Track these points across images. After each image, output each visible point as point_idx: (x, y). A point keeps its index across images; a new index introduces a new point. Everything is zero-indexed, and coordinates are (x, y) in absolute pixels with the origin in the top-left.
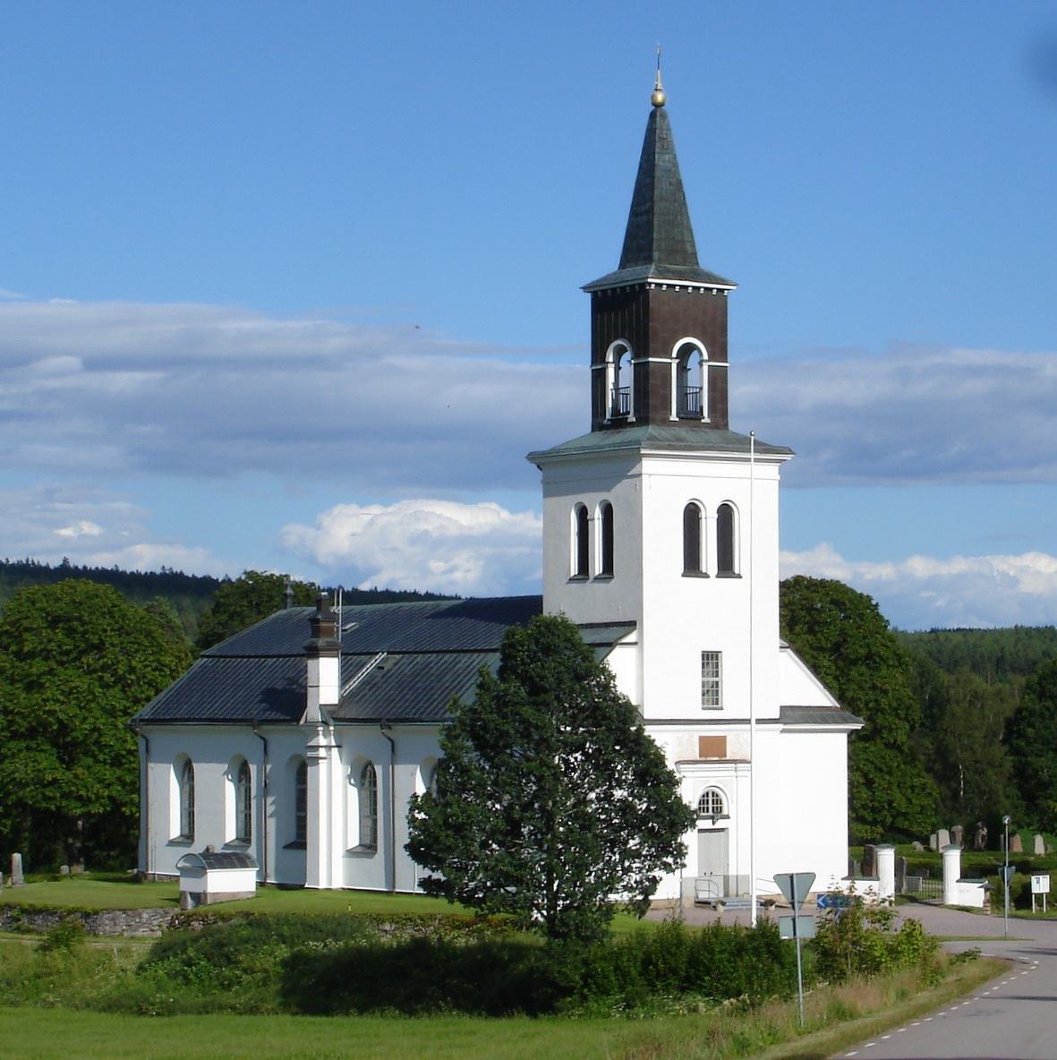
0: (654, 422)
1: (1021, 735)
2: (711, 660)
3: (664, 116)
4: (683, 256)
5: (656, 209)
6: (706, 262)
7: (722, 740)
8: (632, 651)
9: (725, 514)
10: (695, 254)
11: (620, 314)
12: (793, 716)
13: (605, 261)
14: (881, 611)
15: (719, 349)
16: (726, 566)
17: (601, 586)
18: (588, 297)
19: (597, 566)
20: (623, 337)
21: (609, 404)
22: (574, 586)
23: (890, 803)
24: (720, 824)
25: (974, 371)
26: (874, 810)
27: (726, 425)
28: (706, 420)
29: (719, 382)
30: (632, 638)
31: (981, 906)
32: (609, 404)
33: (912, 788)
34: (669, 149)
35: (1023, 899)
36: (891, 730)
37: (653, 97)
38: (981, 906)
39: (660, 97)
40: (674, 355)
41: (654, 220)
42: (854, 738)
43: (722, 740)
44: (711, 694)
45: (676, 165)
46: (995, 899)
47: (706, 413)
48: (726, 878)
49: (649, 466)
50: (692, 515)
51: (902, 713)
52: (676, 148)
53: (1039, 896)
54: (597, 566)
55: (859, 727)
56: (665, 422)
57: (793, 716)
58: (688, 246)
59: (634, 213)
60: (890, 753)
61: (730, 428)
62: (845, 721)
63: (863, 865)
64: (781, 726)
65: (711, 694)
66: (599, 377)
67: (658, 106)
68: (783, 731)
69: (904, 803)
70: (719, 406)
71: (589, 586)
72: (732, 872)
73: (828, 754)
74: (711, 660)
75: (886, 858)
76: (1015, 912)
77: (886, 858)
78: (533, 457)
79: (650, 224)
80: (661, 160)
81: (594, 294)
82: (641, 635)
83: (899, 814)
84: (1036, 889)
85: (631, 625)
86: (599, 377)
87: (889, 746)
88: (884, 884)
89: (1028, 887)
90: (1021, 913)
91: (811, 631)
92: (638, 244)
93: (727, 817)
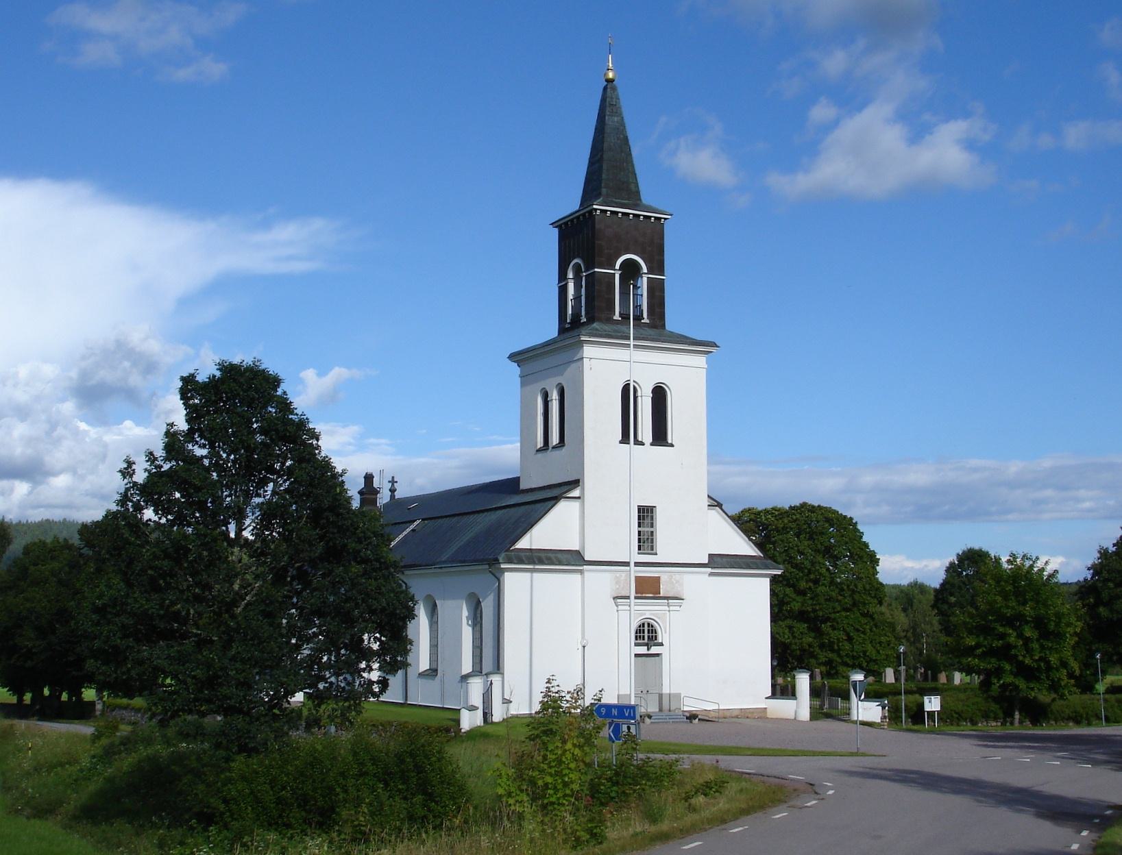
0: (600, 320)
1: (945, 601)
2: (646, 514)
3: (614, 89)
4: (630, 194)
5: (605, 156)
6: (646, 198)
7: (657, 580)
8: (576, 505)
9: (659, 395)
10: (638, 192)
11: (579, 239)
12: (720, 563)
13: (570, 203)
14: (859, 527)
15: (657, 265)
16: (660, 436)
17: (557, 453)
18: (556, 230)
19: (555, 439)
20: (578, 256)
21: (570, 311)
22: (540, 455)
23: (865, 652)
24: (654, 650)
25: (975, 470)
26: (853, 657)
27: (664, 325)
28: (646, 320)
29: (657, 292)
30: (576, 493)
31: (879, 721)
32: (570, 311)
33: (880, 643)
34: (617, 111)
35: (918, 715)
36: (864, 604)
37: (606, 74)
38: (879, 721)
39: (611, 75)
40: (617, 267)
41: (609, 167)
42: (774, 580)
43: (657, 580)
44: (646, 542)
45: (623, 125)
46: (893, 716)
47: (645, 315)
48: (661, 696)
49: (588, 351)
50: (627, 394)
51: (873, 593)
52: (624, 110)
53: (931, 714)
54: (555, 439)
55: (779, 572)
56: (609, 320)
57: (720, 563)
58: (632, 186)
59: (591, 163)
60: (864, 620)
61: (667, 328)
62: (767, 568)
63: (782, 690)
64: (709, 570)
65: (646, 542)
66: (563, 291)
67: (610, 81)
68: (711, 574)
69: (874, 652)
70: (657, 310)
71: (550, 454)
72: (666, 691)
73: (755, 593)
74: (646, 514)
75: (803, 681)
76: (911, 726)
77: (803, 681)
78: (512, 357)
79: (601, 168)
80: (611, 121)
81: (559, 227)
82: (583, 490)
83: (871, 660)
84: (928, 708)
85: (576, 483)
86: (563, 291)
87: (864, 615)
88: (800, 707)
89: (922, 705)
90: (915, 727)
91: (811, 538)
92: (592, 189)
93: (662, 644)
